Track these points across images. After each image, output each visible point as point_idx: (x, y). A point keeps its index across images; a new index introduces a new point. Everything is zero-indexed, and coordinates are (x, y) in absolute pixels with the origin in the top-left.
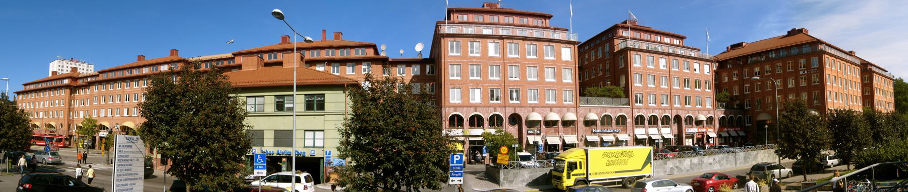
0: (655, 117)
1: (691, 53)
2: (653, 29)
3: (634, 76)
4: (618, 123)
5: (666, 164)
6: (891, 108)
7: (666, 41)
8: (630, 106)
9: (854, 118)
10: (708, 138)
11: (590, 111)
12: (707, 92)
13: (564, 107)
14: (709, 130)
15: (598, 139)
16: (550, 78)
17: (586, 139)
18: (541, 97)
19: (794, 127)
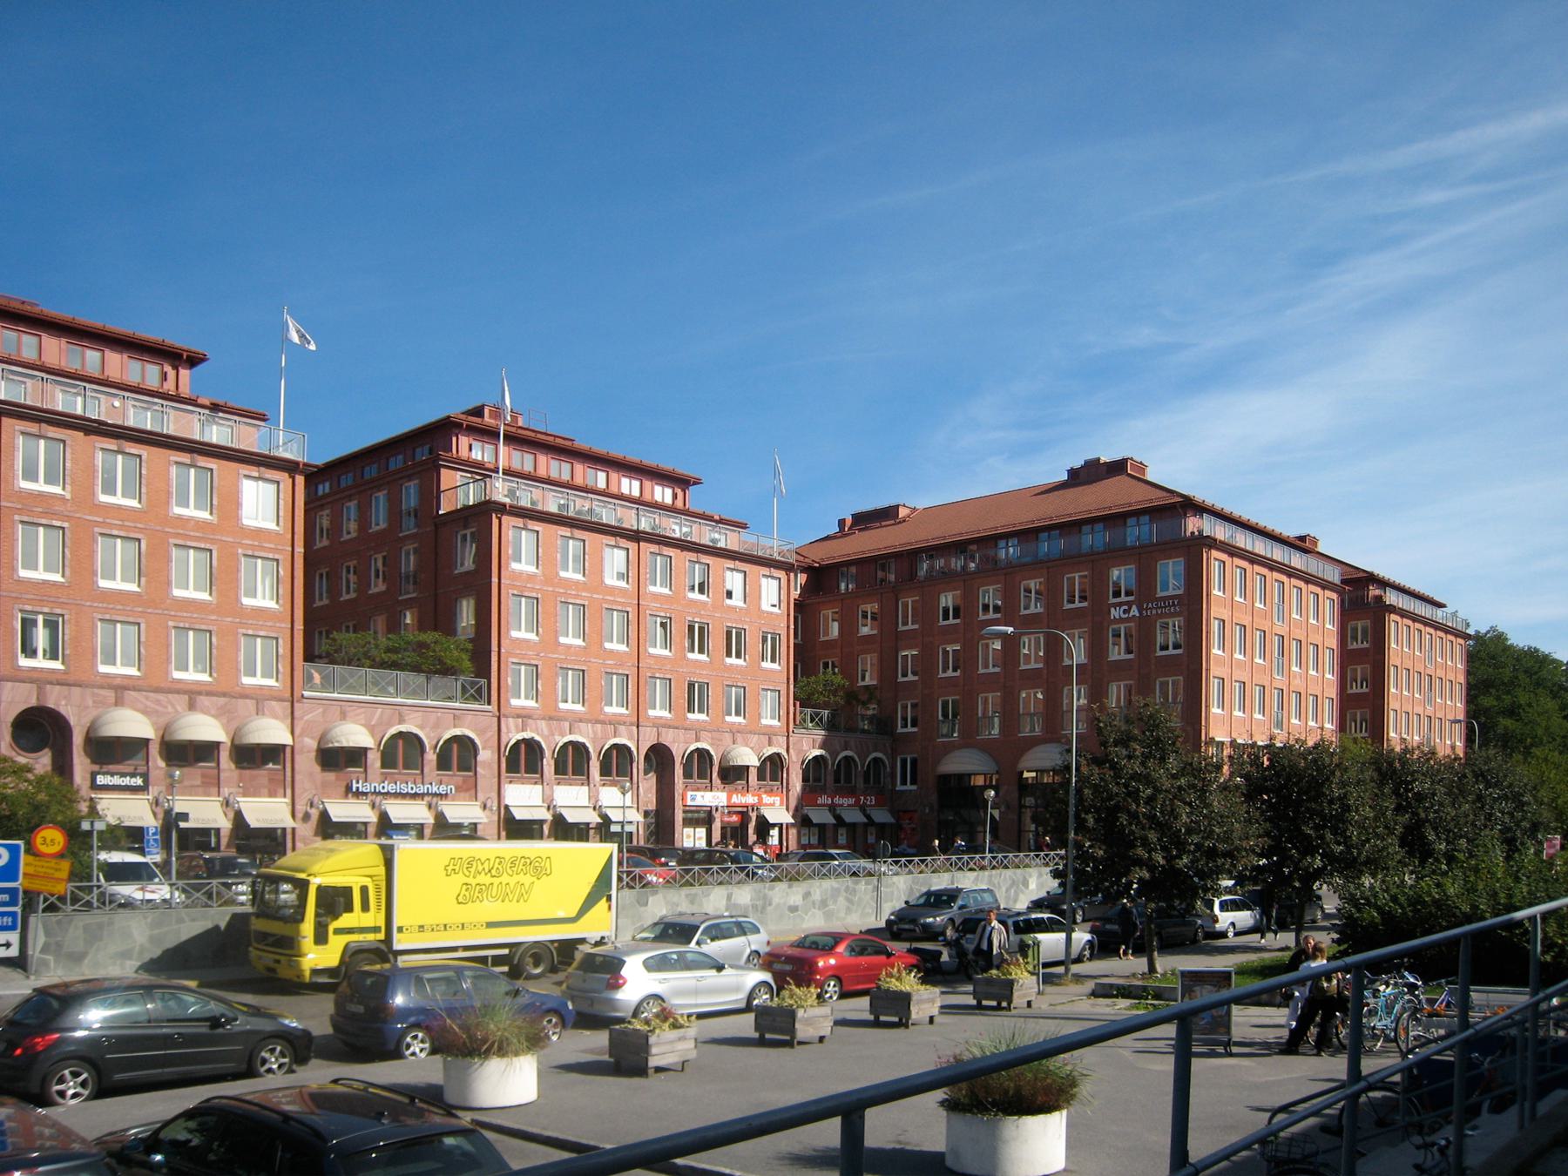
0: (579, 750)
1: (717, 536)
2: (582, 443)
3: (509, 603)
4: (443, 763)
5: (647, 904)
6: (1450, 743)
7: (625, 490)
8: (493, 708)
9: (1338, 773)
10: (764, 827)
11: (343, 716)
12: (766, 670)
13: (246, 696)
14: (766, 799)
15: (372, 817)
16: (190, 590)
17: (324, 815)
18: (153, 655)
19: (1134, 795)
